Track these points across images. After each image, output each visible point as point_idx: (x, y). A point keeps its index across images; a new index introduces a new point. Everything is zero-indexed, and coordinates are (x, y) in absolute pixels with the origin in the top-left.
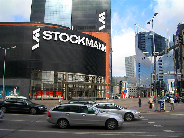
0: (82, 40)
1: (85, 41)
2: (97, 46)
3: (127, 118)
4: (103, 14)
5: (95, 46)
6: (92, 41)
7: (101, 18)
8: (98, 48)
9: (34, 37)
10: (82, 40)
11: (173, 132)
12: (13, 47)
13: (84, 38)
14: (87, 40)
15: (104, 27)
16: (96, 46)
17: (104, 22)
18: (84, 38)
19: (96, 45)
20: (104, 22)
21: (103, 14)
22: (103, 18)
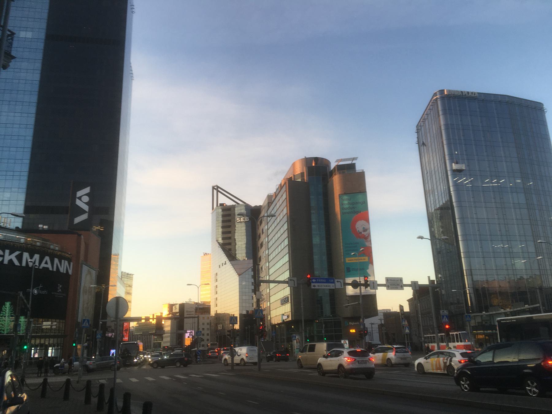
0: (13, 257)
1: (19, 258)
2: (49, 266)
3: (530, 390)
4: (87, 190)
5: (43, 265)
6: (37, 257)
7: (80, 198)
8: (51, 269)
9: (78, 202)
10: (13, 257)
11: (185, 377)
12: (459, 182)
13: (17, 253)
14: (26, 255)
15: (84, 217)
16: (46, 266)
17: (86, 208)
18: (17, 253)
19: (46, 263)
20: (86, 208)
21: (87, 190)
22: (86, 199)
